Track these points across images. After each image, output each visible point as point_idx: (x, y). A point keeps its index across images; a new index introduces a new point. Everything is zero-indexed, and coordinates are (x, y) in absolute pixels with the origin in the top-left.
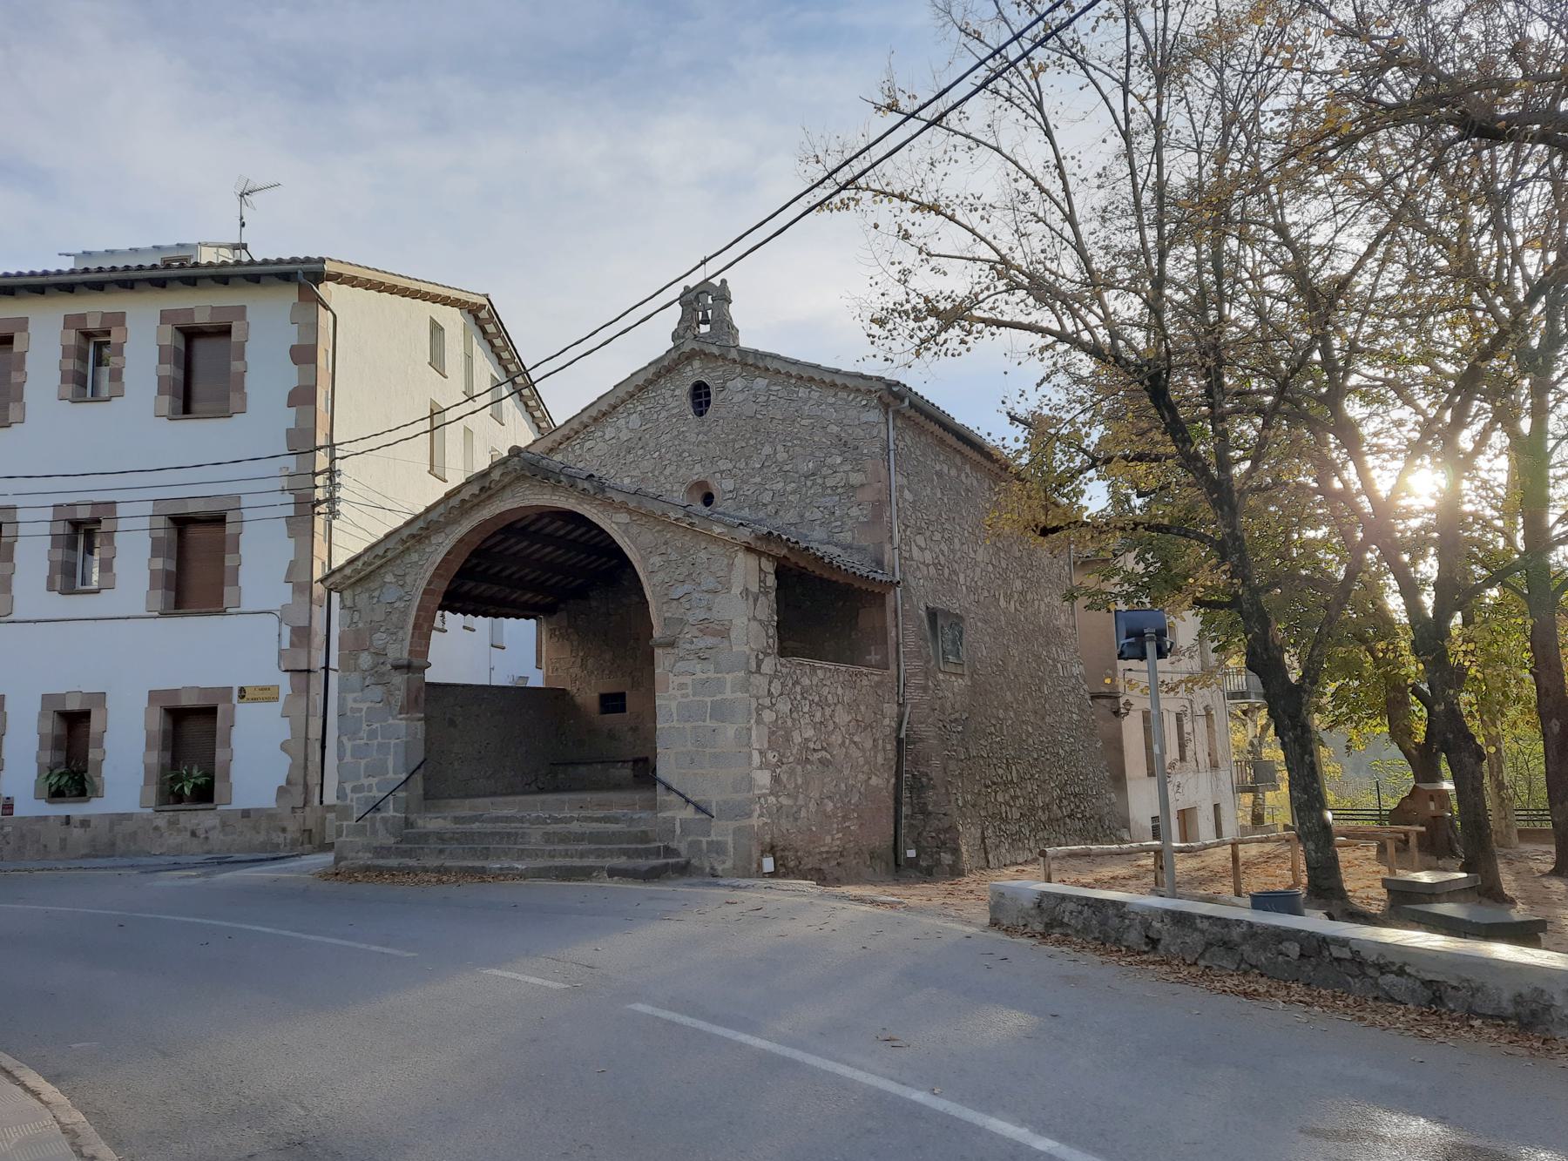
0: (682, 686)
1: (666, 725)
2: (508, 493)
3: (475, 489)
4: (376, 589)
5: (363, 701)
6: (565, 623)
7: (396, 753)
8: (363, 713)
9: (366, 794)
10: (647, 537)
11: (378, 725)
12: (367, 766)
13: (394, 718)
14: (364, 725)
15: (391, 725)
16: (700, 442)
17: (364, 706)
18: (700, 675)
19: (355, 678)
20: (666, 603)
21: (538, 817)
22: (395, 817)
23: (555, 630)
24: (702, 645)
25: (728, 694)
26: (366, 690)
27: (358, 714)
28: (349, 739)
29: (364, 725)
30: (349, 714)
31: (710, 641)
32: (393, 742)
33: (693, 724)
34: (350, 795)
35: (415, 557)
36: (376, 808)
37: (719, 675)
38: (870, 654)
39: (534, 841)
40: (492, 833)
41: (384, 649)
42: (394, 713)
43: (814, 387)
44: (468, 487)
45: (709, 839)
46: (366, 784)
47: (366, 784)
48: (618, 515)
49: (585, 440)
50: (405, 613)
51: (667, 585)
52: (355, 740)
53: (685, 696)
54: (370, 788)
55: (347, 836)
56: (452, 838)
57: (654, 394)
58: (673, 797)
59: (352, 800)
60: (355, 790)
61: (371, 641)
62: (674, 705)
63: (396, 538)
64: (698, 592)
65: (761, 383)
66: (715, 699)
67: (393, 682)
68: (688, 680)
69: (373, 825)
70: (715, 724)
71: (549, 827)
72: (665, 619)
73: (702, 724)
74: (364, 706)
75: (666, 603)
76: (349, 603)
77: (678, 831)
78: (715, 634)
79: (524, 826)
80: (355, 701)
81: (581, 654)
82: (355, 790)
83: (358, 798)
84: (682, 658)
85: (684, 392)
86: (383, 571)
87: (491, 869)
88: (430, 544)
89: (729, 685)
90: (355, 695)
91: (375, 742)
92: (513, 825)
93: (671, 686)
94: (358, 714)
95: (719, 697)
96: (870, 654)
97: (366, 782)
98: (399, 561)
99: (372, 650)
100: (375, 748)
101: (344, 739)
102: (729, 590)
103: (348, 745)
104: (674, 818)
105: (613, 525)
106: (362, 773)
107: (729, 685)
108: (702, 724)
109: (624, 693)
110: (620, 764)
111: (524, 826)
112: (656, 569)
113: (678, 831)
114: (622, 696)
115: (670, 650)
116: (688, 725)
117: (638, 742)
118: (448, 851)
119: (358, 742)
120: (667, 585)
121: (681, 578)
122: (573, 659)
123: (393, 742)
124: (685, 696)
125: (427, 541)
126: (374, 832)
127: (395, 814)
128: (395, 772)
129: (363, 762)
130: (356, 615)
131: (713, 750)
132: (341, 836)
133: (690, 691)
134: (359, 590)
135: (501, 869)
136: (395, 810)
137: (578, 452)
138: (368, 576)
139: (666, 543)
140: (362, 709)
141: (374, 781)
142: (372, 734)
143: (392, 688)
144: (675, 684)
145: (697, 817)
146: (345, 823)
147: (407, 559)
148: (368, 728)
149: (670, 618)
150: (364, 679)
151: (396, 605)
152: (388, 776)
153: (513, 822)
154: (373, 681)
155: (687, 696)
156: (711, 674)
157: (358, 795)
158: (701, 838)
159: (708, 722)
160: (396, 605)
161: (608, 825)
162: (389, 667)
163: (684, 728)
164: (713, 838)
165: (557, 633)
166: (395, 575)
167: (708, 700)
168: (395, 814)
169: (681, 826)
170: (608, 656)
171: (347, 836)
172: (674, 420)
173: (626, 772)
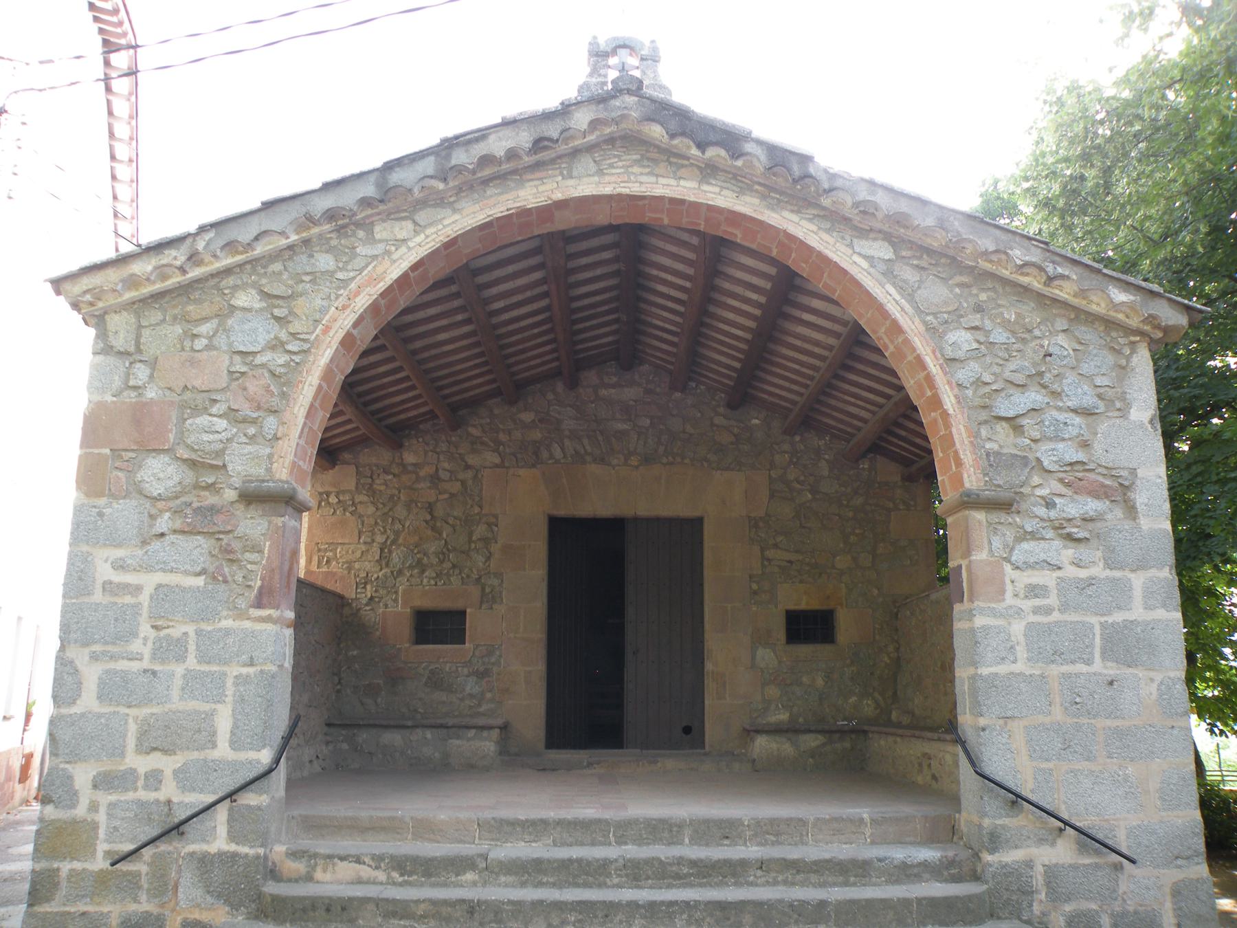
0: (1034, 591)
1: (1002, 669)
2: (585, 163)
3: (524, 139)
4: (206, 319)
5: (146, 568)
6: (351, 484)
8: (144, 598)
9: (143, 795)
11: (190, 629)
13: (241, 615)
17: (150, 581)
18: (1071, 572)
19: (125, 513)
20: (986, 422)
22: (234, 856)
24: (1073, 510)
25: (1137, 612)
26: (156, 545)
27: (128, 599)
29: (145, 629)
31: (1092, 506)
33: (1066, 669)
34: (86, 795)
36: (176, 829)
37: (1117, 574)
41: (220, 453)
44: (507, 132)
46: (142, 770)
47: (142, 770)
48: (863, 242)
50: (285, 380)
51: (987, 389)
54: (154, 779)
58: (1022, 821)
60: (103, 782)
61: (181, 434)
63: (296, 211)
64: (1059, 409)
66: (1110, 620)
67: (240, 531)
68: (1047, 578)
70: (1112, 670)
72: (988, 455)
74: (150, 581)
75: (986, 422)
76: (121, 341)
78: (1098, 492)
80: (119, 566)
81: (380, 539)
82: (103, 782)
84: (1033, 536)
86: (231, 281)
88: (371, 239)
89: (1138, 593)
90: (120, 553)
91: (179, 670)
93: (1009, 587)
94: (128, 599)
95: (1118, 617)
97: (143, 764)
99: (183, 453)
100: (178, 682)
101: (80, 656)
102: (1123, 412)
103: (91, 675)
104: (1029, 864)
105: (856, 258)
107: (1138, 593)
109: (463, 613)
110: (472, 733)
112: (960, 354)
114: (459, 616)
115: (1003, 517)
116: (1055, 670)
117: (489, 695)
119: (122, 665)
120: (987, 389)
121: (1020, 378)
125: (361, 234)
127: (233, 847)
128: (235, 744)
130: (141, 373)
133: (1053, 600)
134: (154, 316)
138: (185, 290)
139: (979, 309)
141: (168, 764)
142: (170, 650)
143: (236, 545)
144: (1020, 586)
145: (1087, 861)
147: (301, 262)
149: (998, 454)
150: (152, 517)
151: (259, 360)
152: (215, 754)
154: (178, 524)
155: (1048, 611)
156: (1098, 571)
159: (1098, 665)
160: (259, 360)
162: (230, 495)
165: (333, 499)
166: (266, 295)
173: (488, 745)
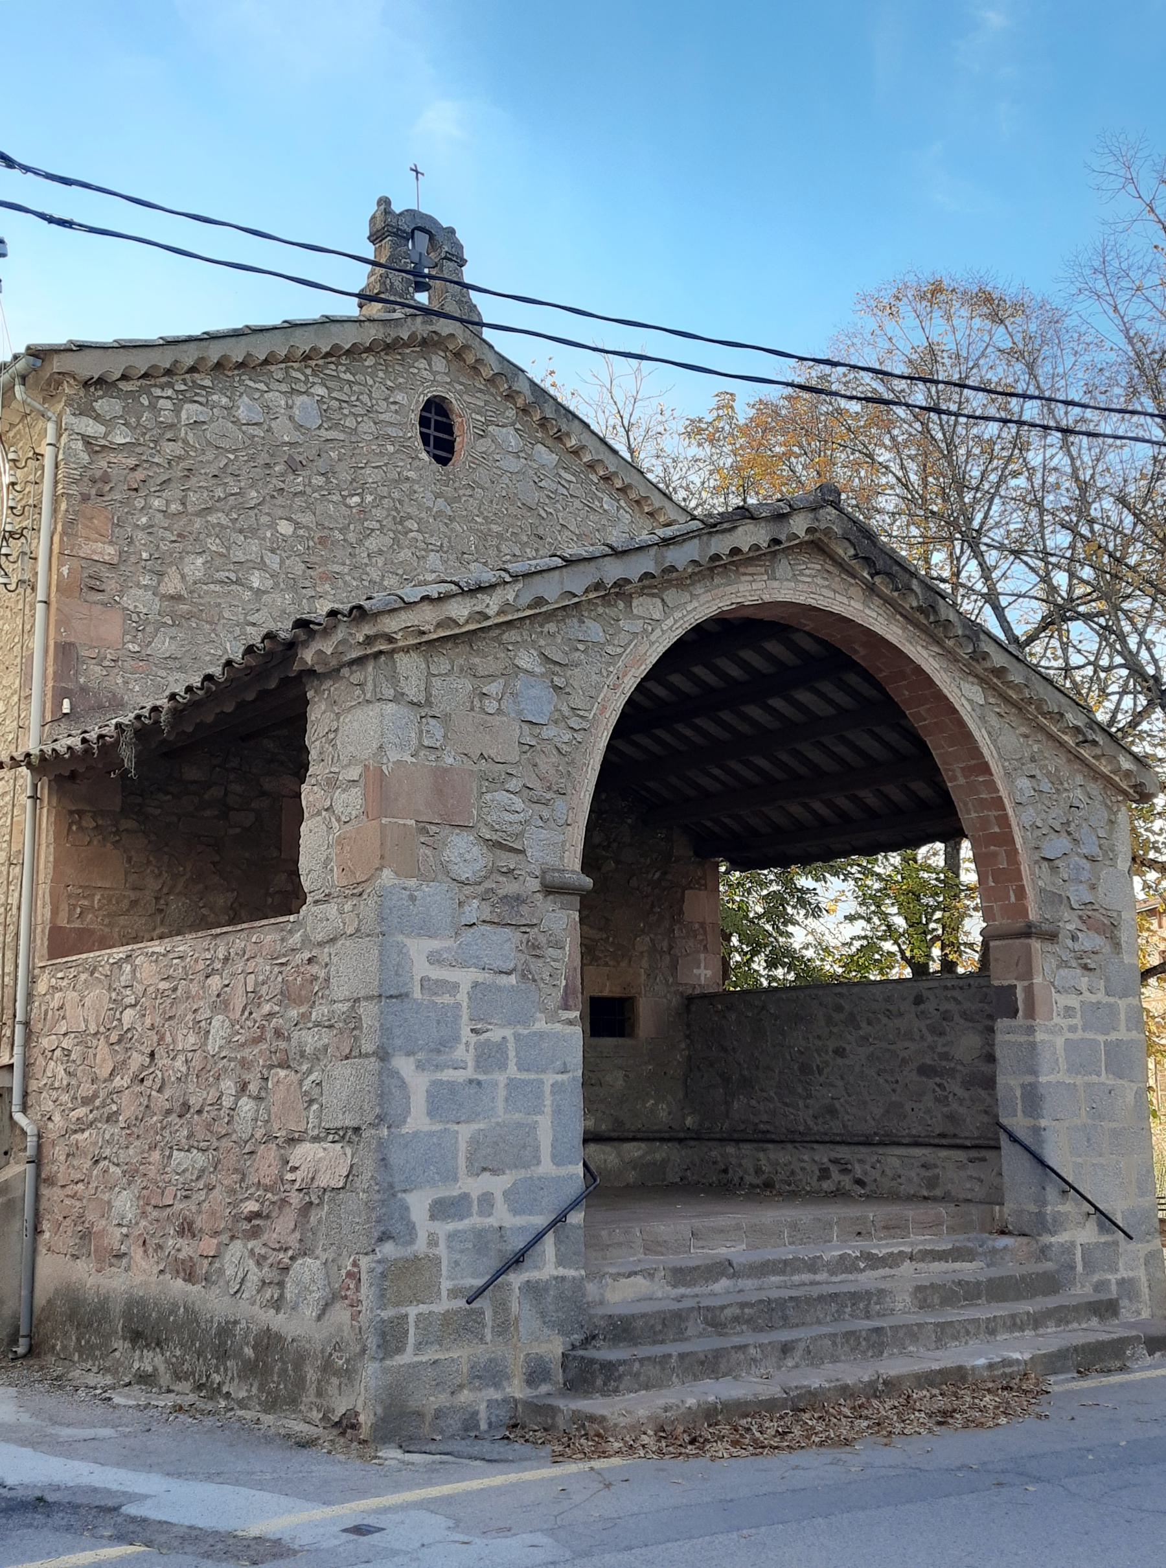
0: (1069, 1011)
7: (557, 1111)
8: (462, 997)
9: (475, 1220)
10: (1011, 739)
11: (508, 1032)
12: (475, 1143)
13: (552, 1018)
14: (465, 1032)
15: (541, 1035)
16: (441, 513)
17: (465, 978)
21: (842, 1257)
23: (80, 813)
26: (468, 935)
27: (447, 999)
28: (420, 1066)
29: (465, 1032)
30: (417, 994)
32: (550, 1078)
35: (594, 630)
37: (1111, 1000)
38: (699, 967)
39: (900, 1306)
40: (821, 1298)
41: (519, 836)
42: (551, 1005)
43: (622, 503)
45: (1118, 1276)
49: (182, 399)
52: (438, 1067)
53: (1073, 1029)
54: (487, 1201)
55: (419, 1347)
56: (736, 1319)
57: (348, 376)
59: (433, 1242)
60: (441, 1210)
62: (1059, 1042)
65: (546, 456)
69: (502, 1307)
71: (862, 1277)
73: (1094, 1078)
74: (465, 978)
77: (1080, 1268)
79: (818, 1277)
80: (434, 959)
83: (451, 1236)
85: (413, 403)
87: (973, 1368)
90: (435, 944)
91: (501, 1078)
92: (796, 1278)
96: (699, 967)
97: (474, 1186)
98: (551, 627)
100: (502, 1093)
104: (1073, 1244)
106: (462, 1162)
108: (1094, 1078)
111: (818, 1277)
113: (1080, 1268)
116: (1079, 1080)
118: (802, 1345)
122: (133, 895)
123: (550, 1078)
124: (1073, 1029)
126: (504, 1327)
127: (561, 1271)
128: (557, 1159)
129: (465, 1132)
131: (1114, 1125)
132: (400, 1350)
133: (1077, 1021)
134: (442, 664)
135: (991, 1366)
136: (561, 1261)
137: (166, 416)
139: (1033, 760)
140: (456, 986)
141: (498, 1184)
142: (490, 1057)
145: (1103, 1240)
146: (413, 1311)
148: (474, 1039)
151: (546, 733)
153: (797, 1271)
156: (1100, 996)
157: (451, 1226)
158: (1110, 1277)
160: (546, 733)
161: (957, 1265)
163: (1074, 1085)
164: (1123, 1273)
167: (1101, 1038)
168: (561, 1271)
169: (1083, 1259)
170: (153, 884)
171: (419, 1347)
172: (391, 449)
